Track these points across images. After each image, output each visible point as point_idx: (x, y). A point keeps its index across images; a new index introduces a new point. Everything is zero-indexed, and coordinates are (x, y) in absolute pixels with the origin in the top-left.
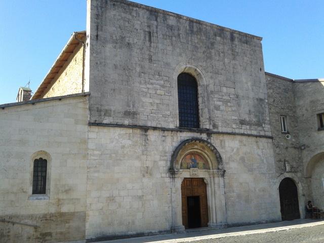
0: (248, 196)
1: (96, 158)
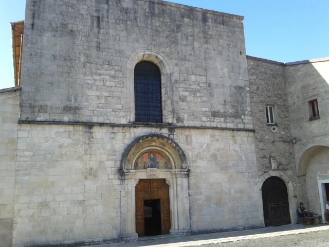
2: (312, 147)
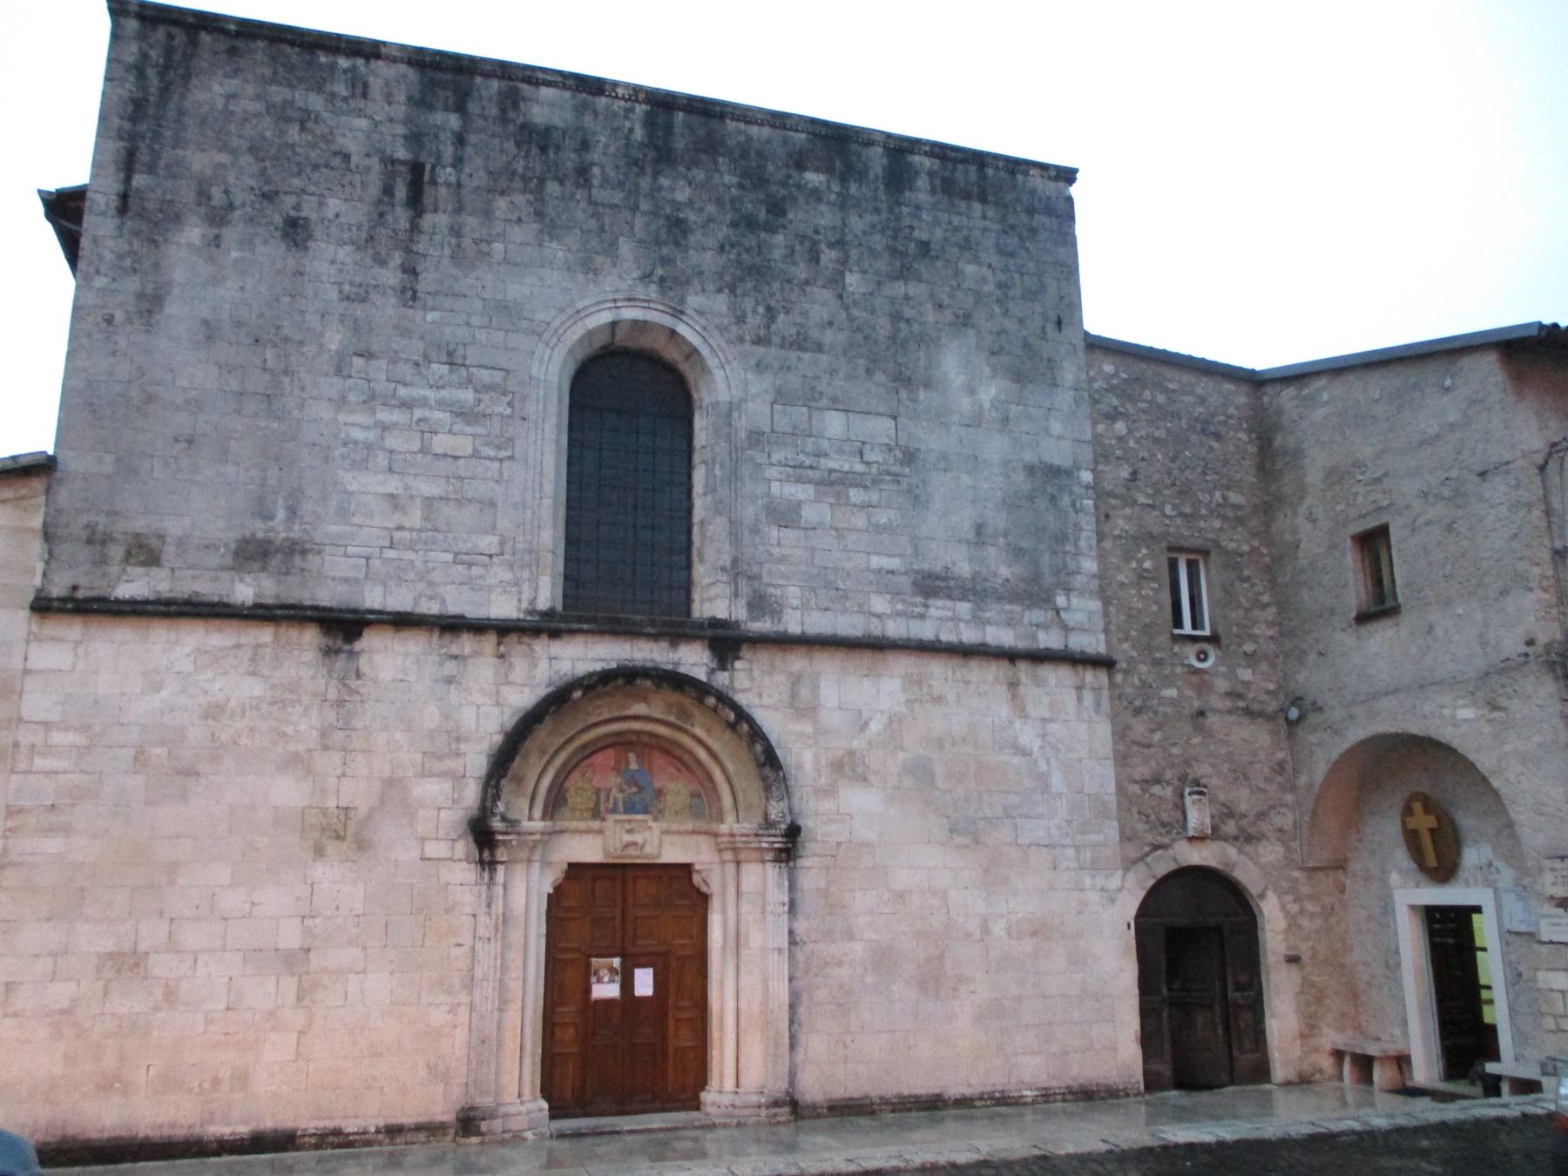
0: (941, 957)
1: (63, 764)
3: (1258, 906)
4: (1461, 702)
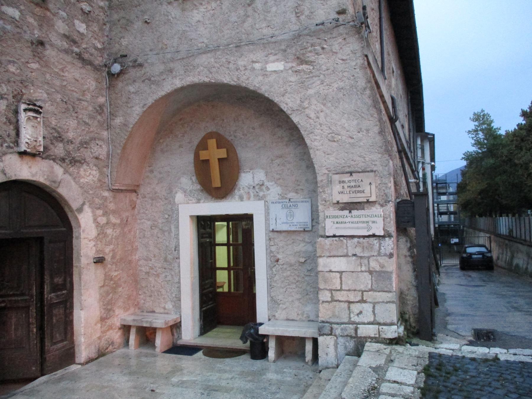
2: (182, 88)
3: (76, 218)
4: (272, 58)
